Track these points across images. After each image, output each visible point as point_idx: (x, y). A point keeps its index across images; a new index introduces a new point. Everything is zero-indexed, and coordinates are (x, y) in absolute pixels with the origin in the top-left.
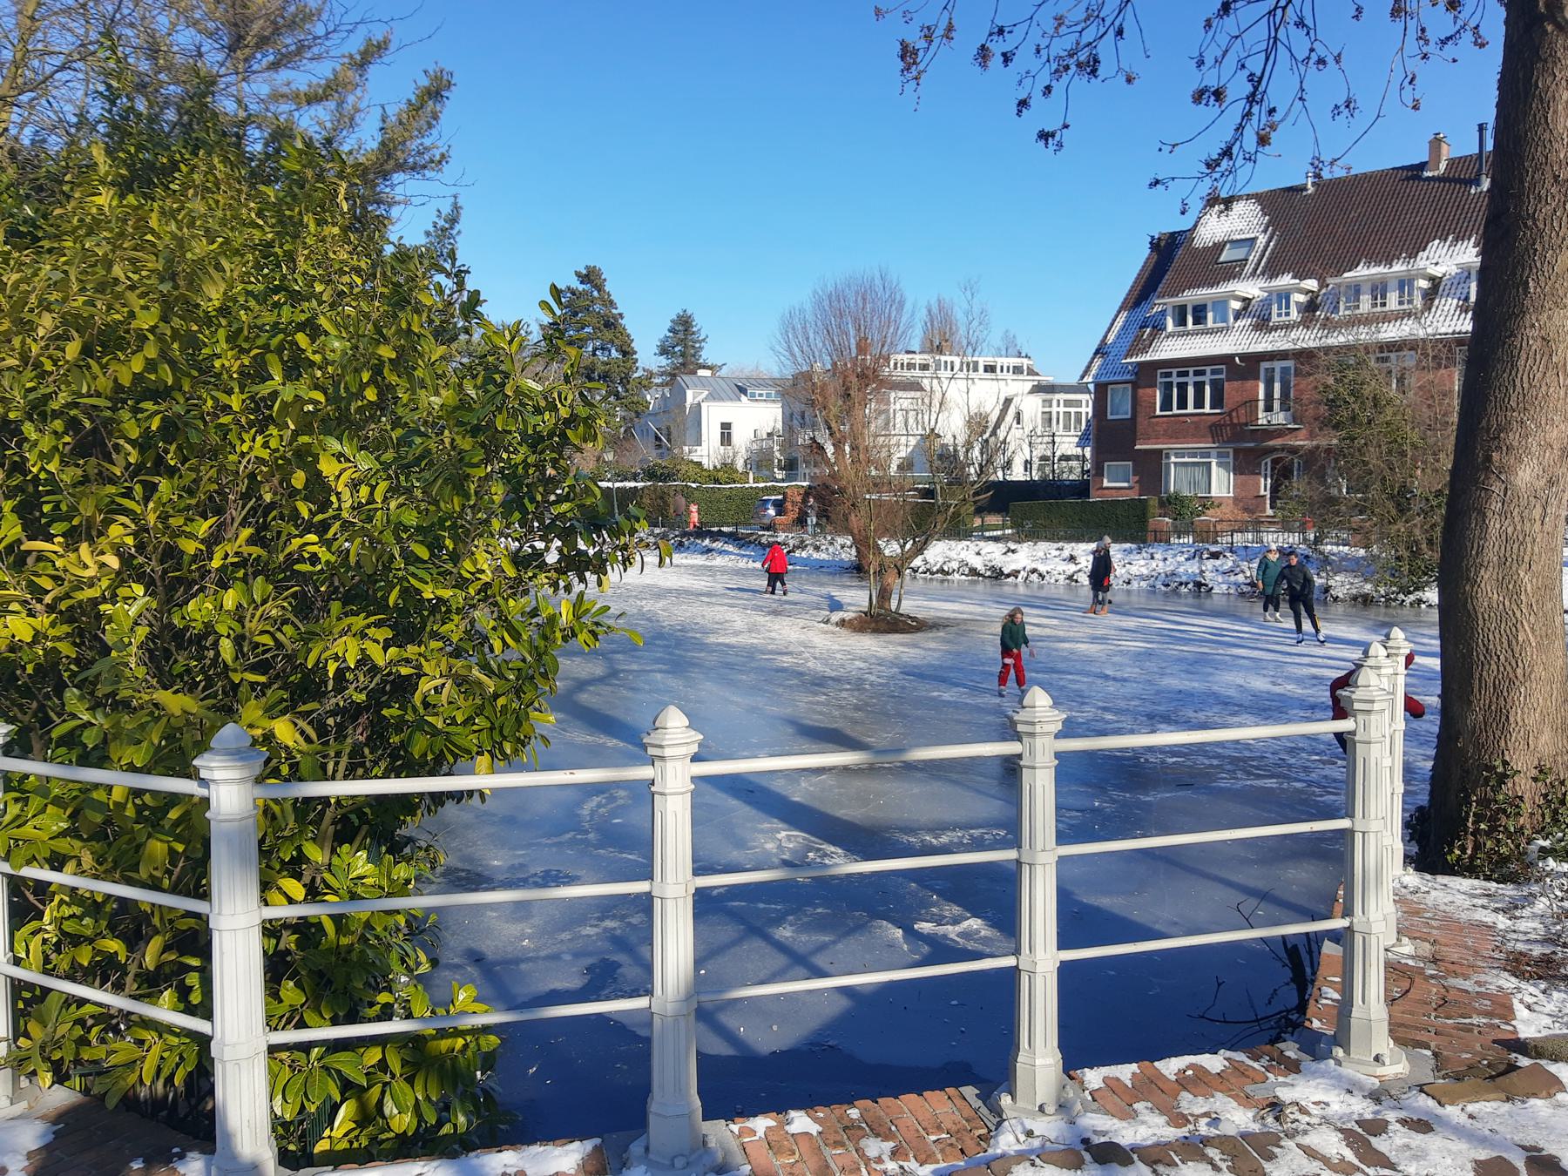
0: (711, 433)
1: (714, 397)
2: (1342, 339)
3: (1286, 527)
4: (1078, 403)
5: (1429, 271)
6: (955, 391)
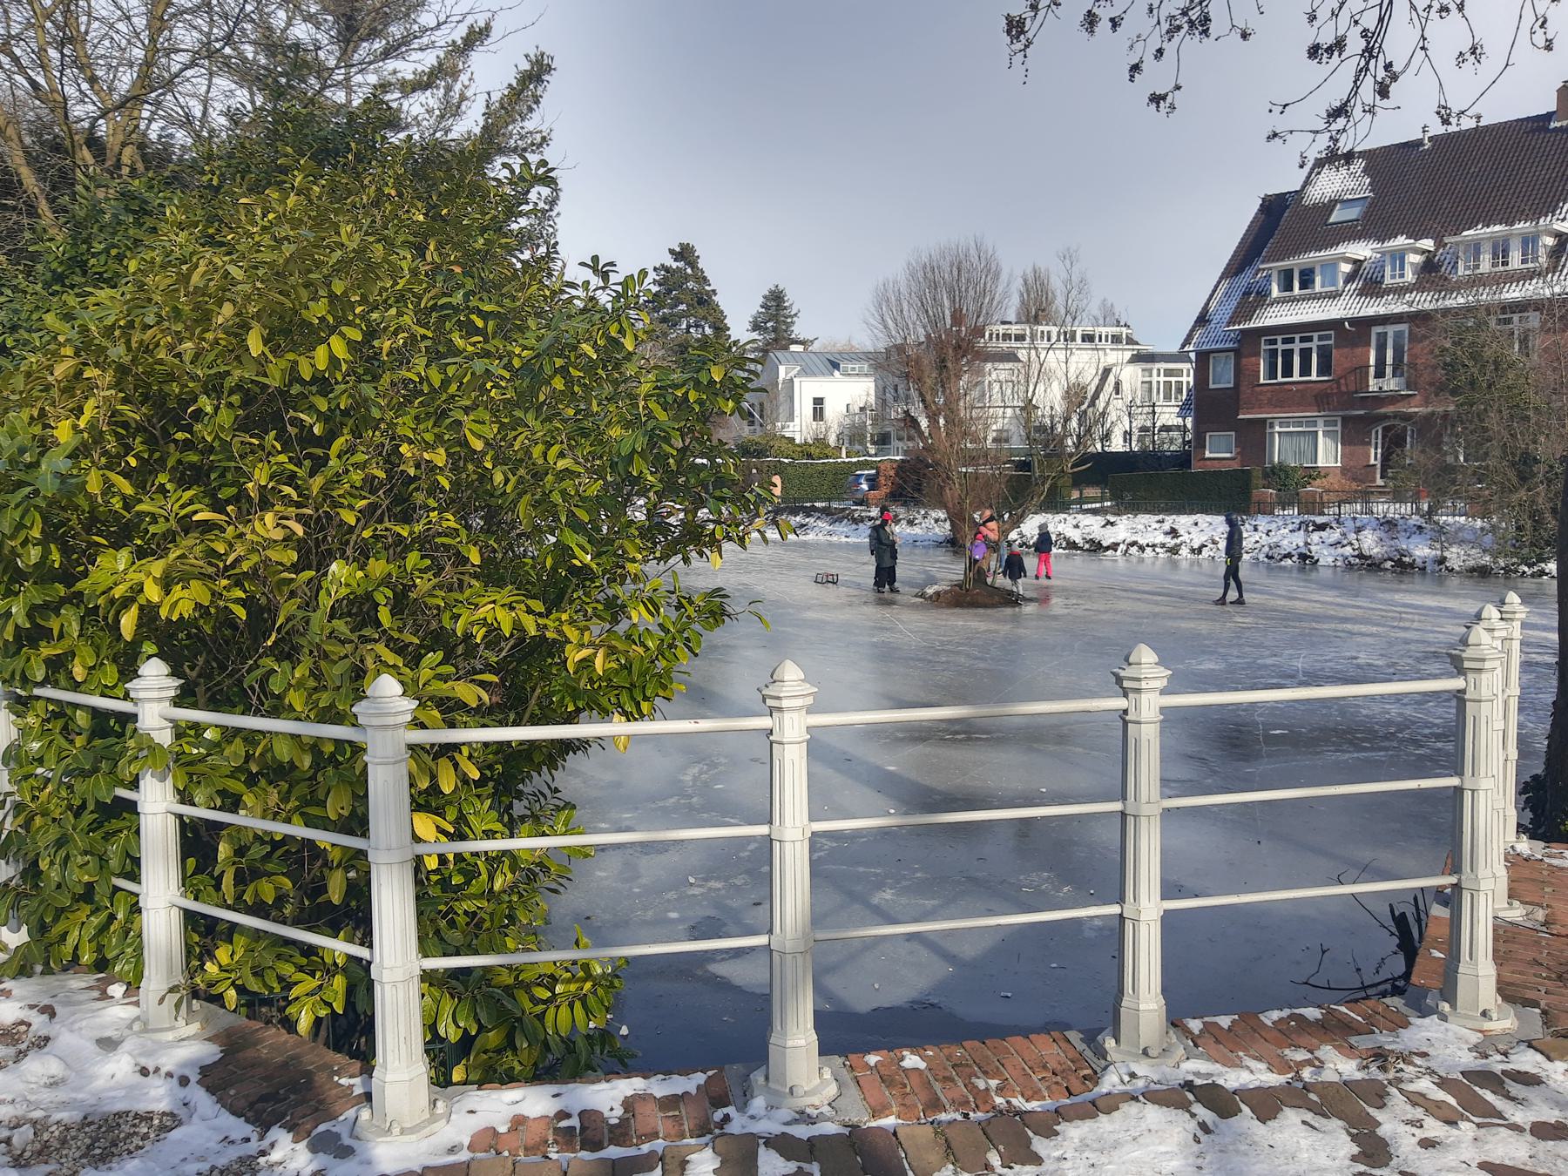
0: (804, 408)
1: (806, 372)
2: (1461, 300)
3: (1397, 497)
4: (1179, 373)
5: (1555, 227)
6: (1054, 359)
